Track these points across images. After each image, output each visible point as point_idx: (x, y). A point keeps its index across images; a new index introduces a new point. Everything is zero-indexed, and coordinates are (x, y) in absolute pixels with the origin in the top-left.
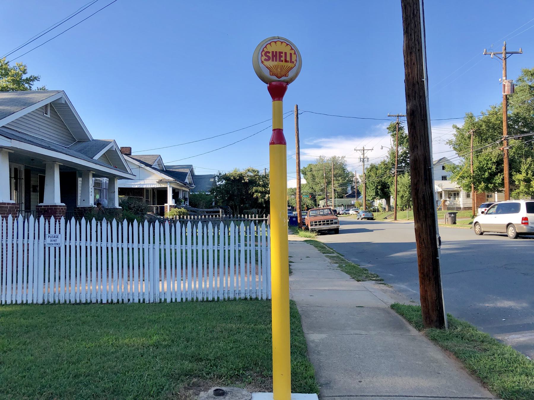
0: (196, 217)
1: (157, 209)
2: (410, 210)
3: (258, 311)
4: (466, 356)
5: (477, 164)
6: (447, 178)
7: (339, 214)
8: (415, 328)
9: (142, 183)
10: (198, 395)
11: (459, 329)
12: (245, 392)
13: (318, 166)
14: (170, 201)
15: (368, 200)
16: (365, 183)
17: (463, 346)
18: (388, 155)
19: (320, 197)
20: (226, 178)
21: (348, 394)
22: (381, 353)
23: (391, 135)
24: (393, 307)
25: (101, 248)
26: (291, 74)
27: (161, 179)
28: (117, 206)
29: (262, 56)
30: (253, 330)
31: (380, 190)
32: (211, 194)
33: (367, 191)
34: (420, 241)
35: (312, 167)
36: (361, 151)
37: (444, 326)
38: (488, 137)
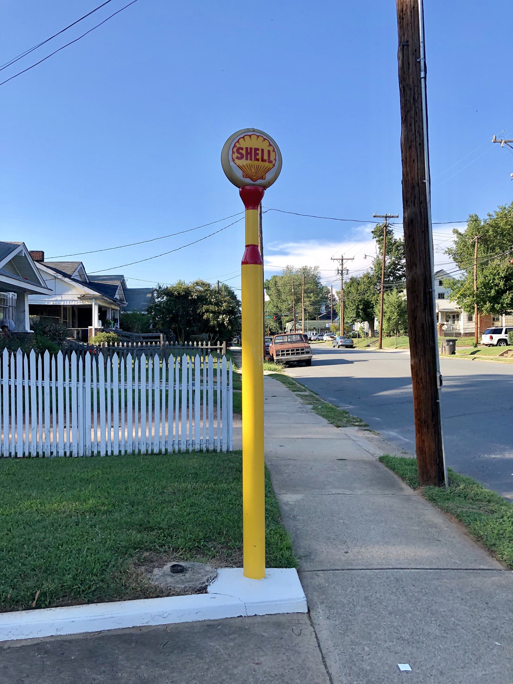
0: (130, 344)
1: (78, 333)
2: (399, 336)
3: (217, 466)
4: (471, 520)
5: (481, 279)
6: (445, 296)
7: (310, 340)
8: (410, 485)
9: (58, 299)
10: (151, 572)
11: (462, 487)
12: (208, 568)
13: (284, 278)
14: (96, 323)
15: (347, 323)
16: (344, 302)
17: (466, 507)
18: (373, 266)
19: (287, 318)
20: (167, 292)
21: (333, 568)
22: (369, 517)
23: (377, 241)
24: (381, 459)
25: (16, 386)
26: (269, 176)
27: (84, 293)
28: (28, 329)
29: (233, 152)
30: (214, 491)
31: (361, 311)
32: (149, 314)
33: (346, 312)
34: (417, 381)
35: (277, 280)
36: (339, 260)
37: (444, 483)
38: (496, 246)
